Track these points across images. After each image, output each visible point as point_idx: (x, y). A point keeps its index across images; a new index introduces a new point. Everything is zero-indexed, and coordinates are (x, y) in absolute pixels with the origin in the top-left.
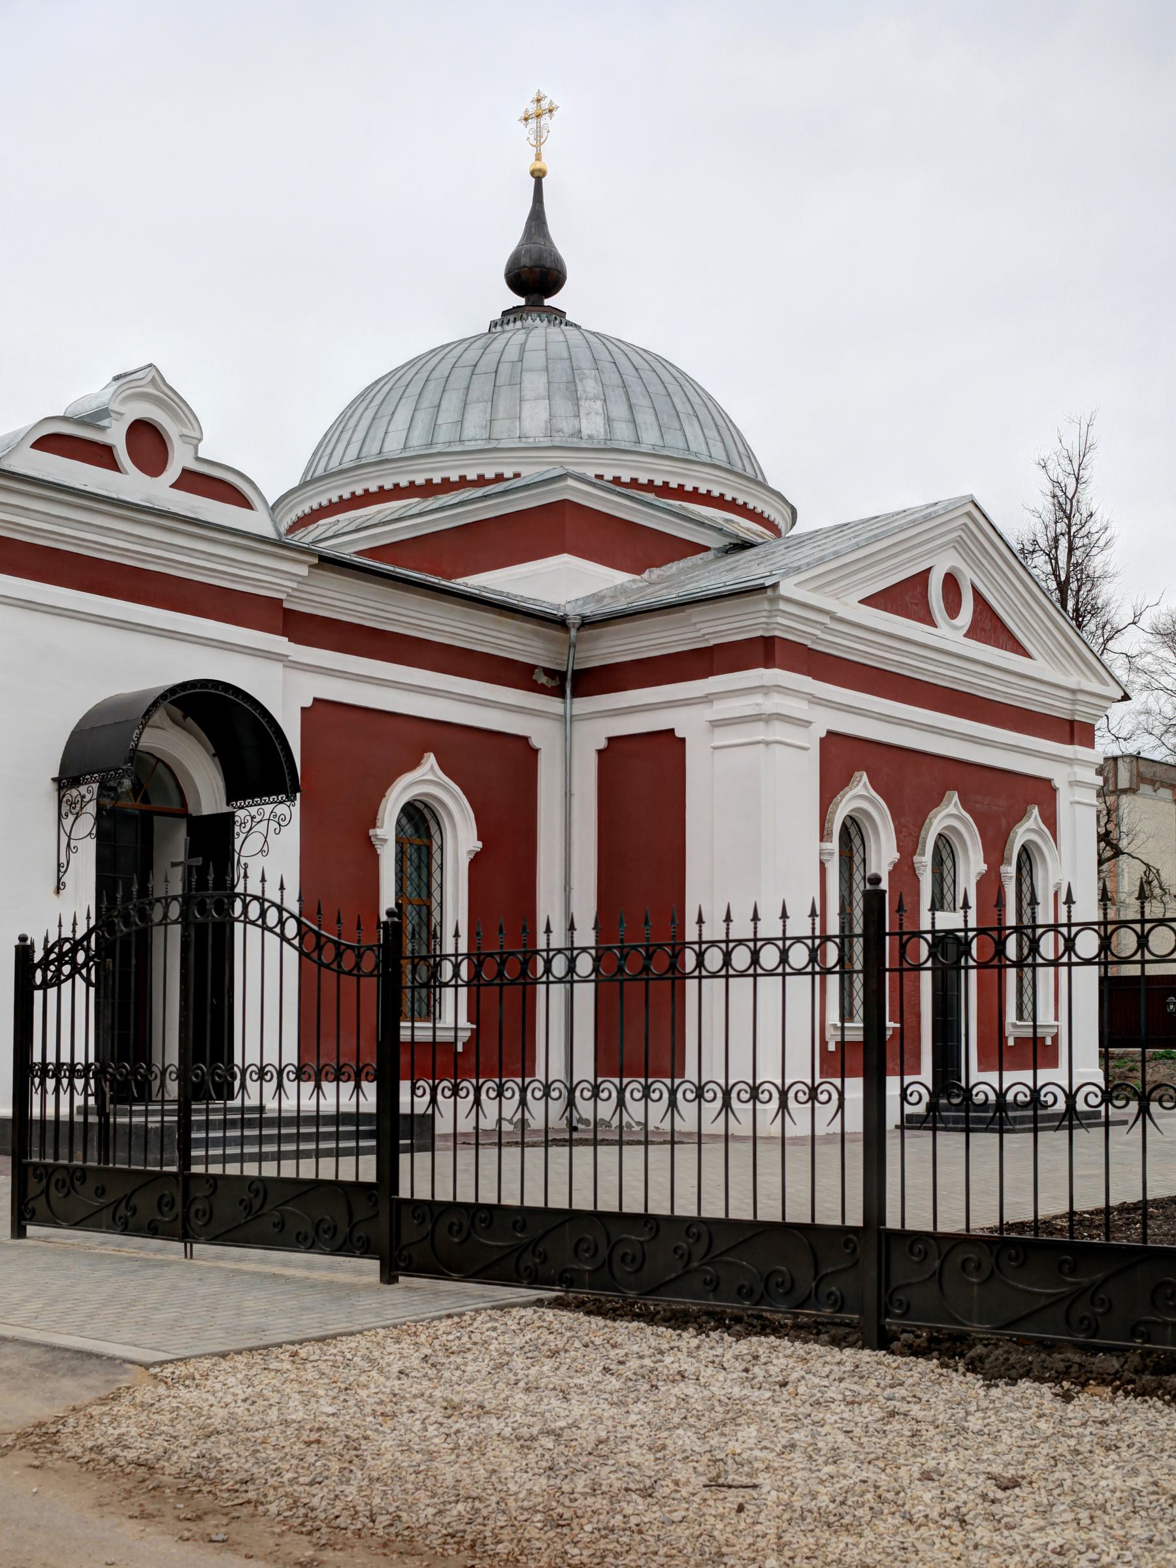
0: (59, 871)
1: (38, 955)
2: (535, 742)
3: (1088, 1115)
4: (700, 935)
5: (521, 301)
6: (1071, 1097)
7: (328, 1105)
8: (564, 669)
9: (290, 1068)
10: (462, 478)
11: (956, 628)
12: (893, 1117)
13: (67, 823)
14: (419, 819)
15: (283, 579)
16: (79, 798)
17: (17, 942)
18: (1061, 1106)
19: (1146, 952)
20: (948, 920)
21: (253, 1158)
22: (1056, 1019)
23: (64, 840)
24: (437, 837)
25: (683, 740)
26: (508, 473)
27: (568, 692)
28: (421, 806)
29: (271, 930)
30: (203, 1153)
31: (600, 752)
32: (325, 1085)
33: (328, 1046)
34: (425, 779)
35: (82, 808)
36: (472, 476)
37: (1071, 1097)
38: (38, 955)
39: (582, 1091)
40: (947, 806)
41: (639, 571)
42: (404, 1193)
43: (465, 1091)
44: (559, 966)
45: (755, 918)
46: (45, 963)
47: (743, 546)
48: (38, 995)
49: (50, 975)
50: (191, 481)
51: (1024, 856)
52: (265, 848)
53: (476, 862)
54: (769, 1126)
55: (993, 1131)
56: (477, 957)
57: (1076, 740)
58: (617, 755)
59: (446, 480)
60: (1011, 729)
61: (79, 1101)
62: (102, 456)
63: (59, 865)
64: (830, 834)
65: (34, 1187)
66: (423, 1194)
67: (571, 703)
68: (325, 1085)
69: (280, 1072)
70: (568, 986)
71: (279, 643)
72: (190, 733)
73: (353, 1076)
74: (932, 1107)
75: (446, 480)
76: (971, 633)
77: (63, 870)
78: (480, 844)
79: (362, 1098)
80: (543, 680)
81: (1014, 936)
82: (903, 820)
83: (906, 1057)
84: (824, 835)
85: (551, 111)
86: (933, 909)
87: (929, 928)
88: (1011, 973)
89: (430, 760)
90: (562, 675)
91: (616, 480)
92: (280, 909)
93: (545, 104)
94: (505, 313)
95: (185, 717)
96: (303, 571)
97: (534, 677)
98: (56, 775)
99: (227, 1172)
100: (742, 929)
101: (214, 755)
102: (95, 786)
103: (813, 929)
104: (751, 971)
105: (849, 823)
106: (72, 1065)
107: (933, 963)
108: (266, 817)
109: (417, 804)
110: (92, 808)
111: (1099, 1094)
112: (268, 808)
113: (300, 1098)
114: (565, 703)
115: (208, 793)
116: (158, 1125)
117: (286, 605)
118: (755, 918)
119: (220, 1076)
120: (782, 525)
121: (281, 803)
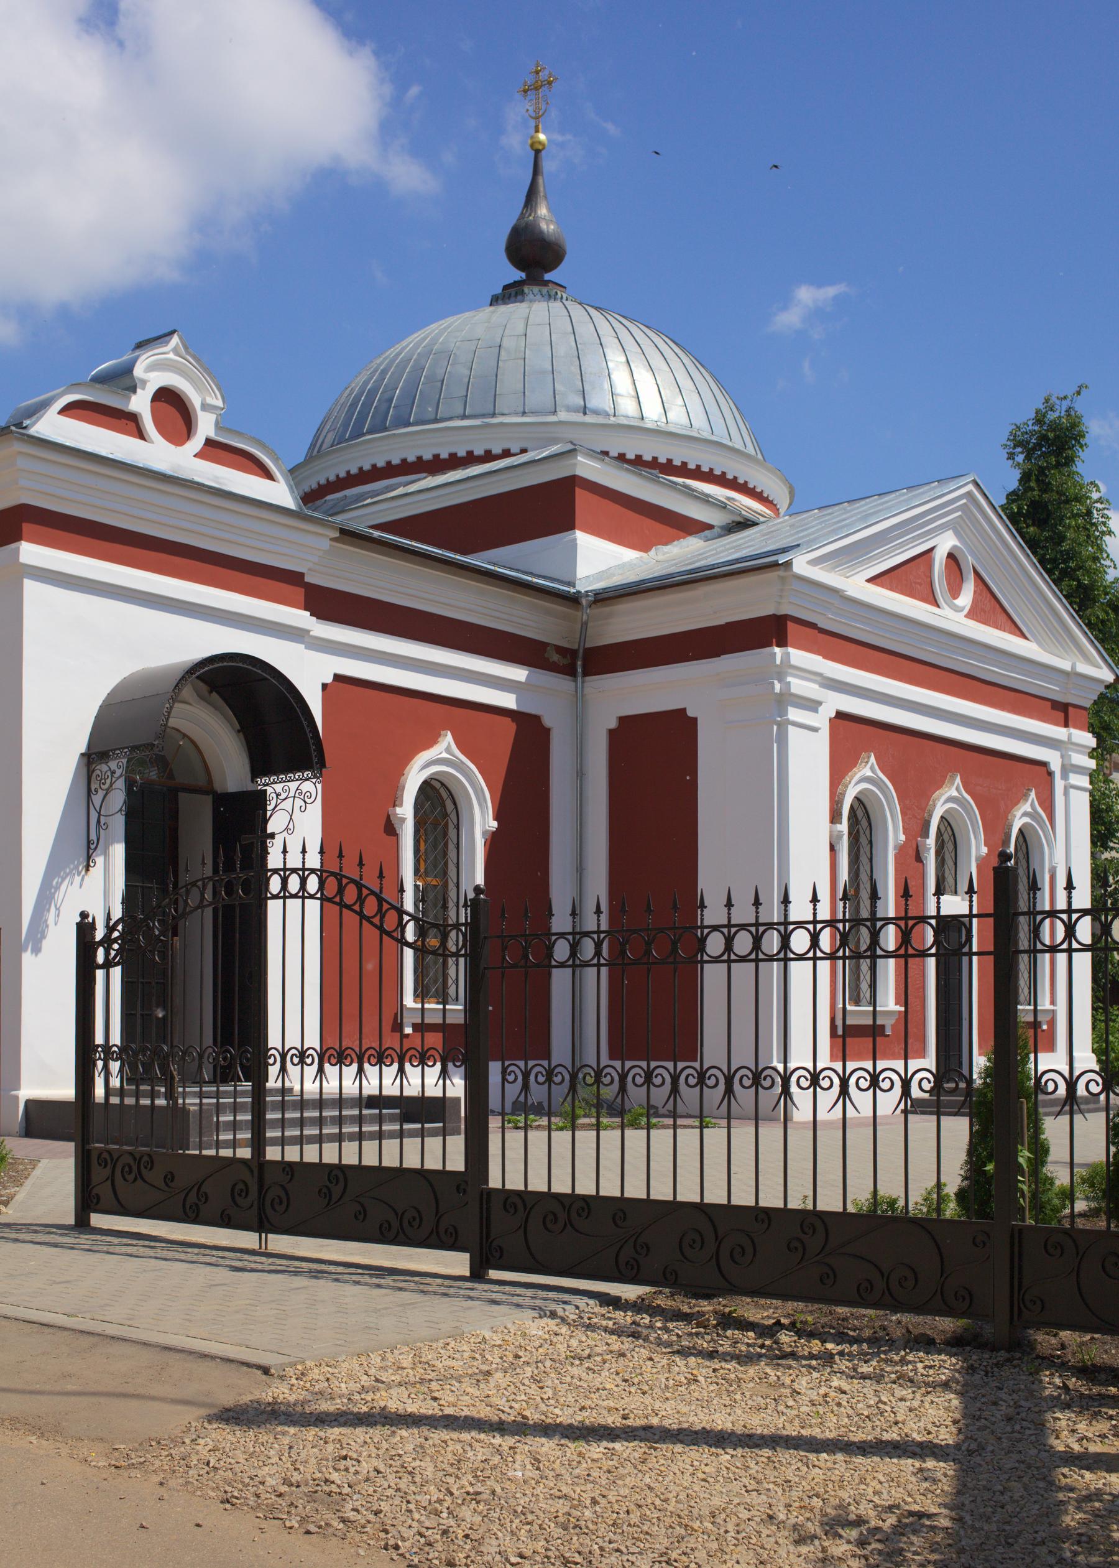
0: (89, 848)
1: (99, 934)
2: (547, 722)
3: (1086, 1101)
4: (815, 914)
6: (1071, 1085)
7: (371, 1087)
8: (576, 647)
9: (294, 1051)
10: (470, 453)
11: (958, 609)
12: (494, 1101)
13: (97, 799)
14: (437, 800)
15: (313, 554)
16: (109, 773)
17: (78, 919)
18: (1062, 1091)
19: (1074, 942)
20: (954, 905)
21: (293, 1141)
22: (1053, 1002)
23: (94, 816)
24: (453, 816)
25: (695, 720)
27: (580, 670)
28: (437, 785)
29: (349, 907)
30: (231, 1137)
33: (350, 1027)
34: (438, 757)
35: (111, 785)
37: (1071, 1085)
38: (99, 934)
39: (536, 1077)
40: (950, 788)
41: (645, 548)
42: (494, 1182)
43: (560, 1077)
44: (588, 948)
45: (729, 904)
46: (107, 941)
48: (100, 974)
49: (113, 953)
50: (213, 450)
51: (1021, 839)
52: (291, 826)
53: (494, 842)
54: (829, 1114)
55: (931, 1113)
57: (1070, 723)
59: (453, 456)
60: (1009, 711)
61: (115, 1082)
62: (129, 423)
63: (89, 842)
64: (840, 815)
65: (99, 1174)
66: (515, 1183)
67: (583, 682)
69: (283, 1056)
70: (902, 961)
71: (300, 618)
72: (216, 708)
73: (356, 1059)
74: (937, 1089)
77: (93, 847)
79: (364, 1082)
80: (555, 658)
81: (828, 930)
82: (907, 802)
83: (910, 1041)
84: (835, 817)
85: (550, 83)
86: (939, 892)
87: (934, 913)
89: (448, 739)
90: (573, 653)
91: (622, 457)
92: (360, 886)
94: (506, 287)
95: (211, 692)
96: (326, 544)
97: (546, 655)
98: (83, 751)
99: (238, 1156)
100: (743, 913)
101: (239, 731)
102: (125, 761)
103: (971, 907)
104: (811, 954)
105: (856, 806)
106: (107, 1047)
107: (937, 950)
108: (291, 794)
109: (434, 783)
110: (120, 784)
111: (868, 1078)
112: (293, 786)
113: (342, 1081)
114: (576, 681)
115: (232, 768)
116: (196, 1108)
118: (729, 904)
119: (247, 1060)
121: (306, 780)
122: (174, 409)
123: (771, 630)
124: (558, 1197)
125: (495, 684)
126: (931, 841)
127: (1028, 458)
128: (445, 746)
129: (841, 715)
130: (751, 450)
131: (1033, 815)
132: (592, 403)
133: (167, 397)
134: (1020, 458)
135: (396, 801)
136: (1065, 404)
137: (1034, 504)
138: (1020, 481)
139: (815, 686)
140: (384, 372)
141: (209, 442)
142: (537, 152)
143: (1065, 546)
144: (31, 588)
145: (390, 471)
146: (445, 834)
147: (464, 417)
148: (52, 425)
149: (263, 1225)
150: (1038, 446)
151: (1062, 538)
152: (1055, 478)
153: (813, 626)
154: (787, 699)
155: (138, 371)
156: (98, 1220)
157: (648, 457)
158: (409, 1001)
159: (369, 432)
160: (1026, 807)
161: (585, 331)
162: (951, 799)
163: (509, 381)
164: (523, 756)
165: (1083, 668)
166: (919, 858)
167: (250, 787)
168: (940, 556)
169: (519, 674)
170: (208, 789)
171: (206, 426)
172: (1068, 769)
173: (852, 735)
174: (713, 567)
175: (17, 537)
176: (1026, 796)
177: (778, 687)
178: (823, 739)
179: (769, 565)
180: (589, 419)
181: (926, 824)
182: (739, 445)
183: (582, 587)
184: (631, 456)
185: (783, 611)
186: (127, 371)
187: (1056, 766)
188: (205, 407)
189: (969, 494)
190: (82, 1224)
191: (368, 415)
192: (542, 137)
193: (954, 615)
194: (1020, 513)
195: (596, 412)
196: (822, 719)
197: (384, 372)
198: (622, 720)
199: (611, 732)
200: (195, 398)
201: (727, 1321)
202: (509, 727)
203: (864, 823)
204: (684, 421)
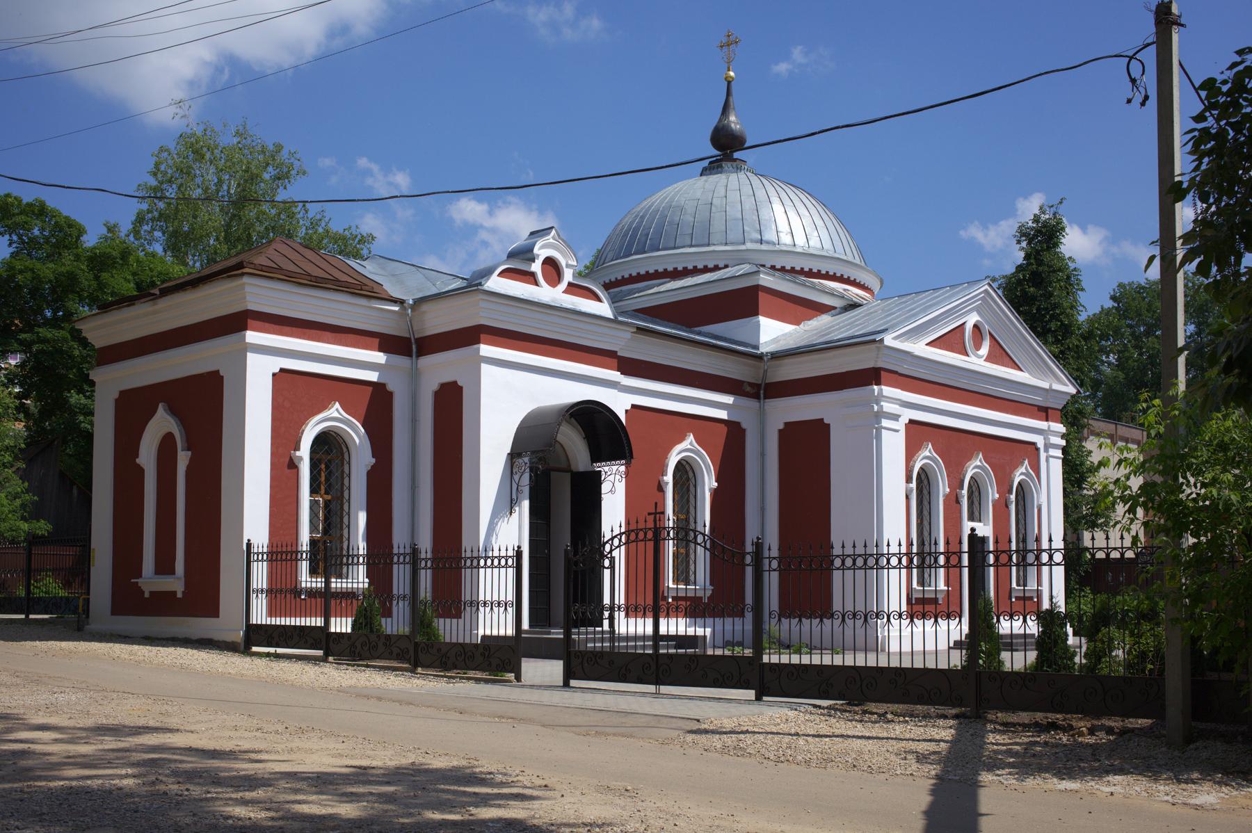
2: (744, 426)
5: (718, 153)
10: (695, 267)
11: (980, 357)
13: (516, 477)
14: (685, 471)
15: (624, 342)
26: (721, 265)
32: (804, 620)
34: (685, 448)
41: (798, 323)
47: (853, 306)
50: (572, 288)
53: (716, 494)
56: (781, 559)
62: (530, 278)
68: (804, 620)
71: (615, 375)
75: (685, 268)
76: (989, 359)
78: (374, 461)
80: (748, 389)
84: (909, 480)
88: (1014, 569)
90: (758, 386)
96: (628, 335)
112: (615, 468)
122: (553, 269)
123: (873, 376)
124: (794, 665)
125: (714, 406)
126: (965, 492)
127: (1029, 243)
128: (689, 442)
129: (911, 421)
130: (857, 261)
131: (1027, 474)
132: (766, 237)
133: (550, 262)
134: (1024, 244)
135: (664, 473)
136: (1053, 210)
137: (1033, 273)
138: (1025, 259)
139: (897, 406)
140: (643, 217)
141: (570, 284)
142: (729, 83)
143: (1053, 300)
144: (485, 368)
145: (648, 277)
146: (688, 490)
147: (691, 246)
148: (496, 283)
149: (658, 682)
150: (1035, 236)
151: (1051, 295)
152: (1046, 257)
153: (896, 373)
154: (881, 415)
155: (536, 251)
156: (573, 683)
157: (798, 268)
158: (1014, 585)
159: (636, 253)
160: (1023, 470)
161: (760, 193)
162: (977, 467)
163: (718, 225)
164: (731, 445)
165: (1056, 386)
166: (958, 502)
167: (590, 469)
168: (969, 327)
169: (728, 399)
170: (568, 470)
171: (568, 276)
172: (1048, 446)
173: (918, 433)
174: (839, 340)
175: (477, 341)
176: (1022, 463)
177: (876, 408)
178: (901, 436)
179: (871, 341)
180: (764, 247)
181: (962, 482)
182: (850, 258)
183: (763, 349)
184: (788, 268)
185: (880, 364)
186: (530, 249)
187: (1041, 445)
188: (568, 266)
189: (986, 291)
190: (566, 684)
191: (633, 239)
192: (732, 74)
193: (978, 361)
194: (1024, 279)
195: (768, 243)
196: (901, 425)
197: (643, 217)
198: (786, 424)
199: (780, 431)
200: (562, 261)
201: (865, 712)
202: (724, 429)
203: (925, 482)
204: (819, 246)
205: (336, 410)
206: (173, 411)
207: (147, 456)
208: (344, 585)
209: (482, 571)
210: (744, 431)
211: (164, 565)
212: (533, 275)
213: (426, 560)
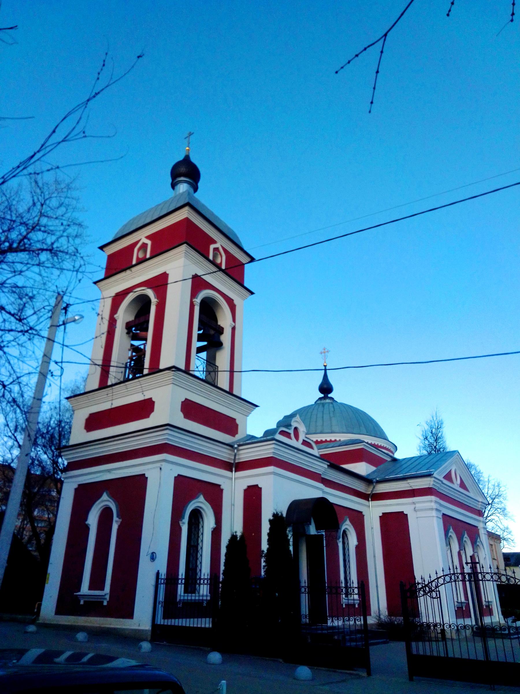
5: (322, 395)
27: (234, 469)
31: (380, 517)
36: (328, 439)
58: (386, 519)
62: (288, 435)
78: (87, 523)
93: (326, 350)
96: (326, 466)
117: (322, 476)
120: (394, 451)
205: (201, 498)
206: (113, 496)
207: (93, 520)
208: (193, 598)
209: (202, 586)
210: (80, 485)
211: (97, 582)
212: (290, 434)
213: (182, 579)
